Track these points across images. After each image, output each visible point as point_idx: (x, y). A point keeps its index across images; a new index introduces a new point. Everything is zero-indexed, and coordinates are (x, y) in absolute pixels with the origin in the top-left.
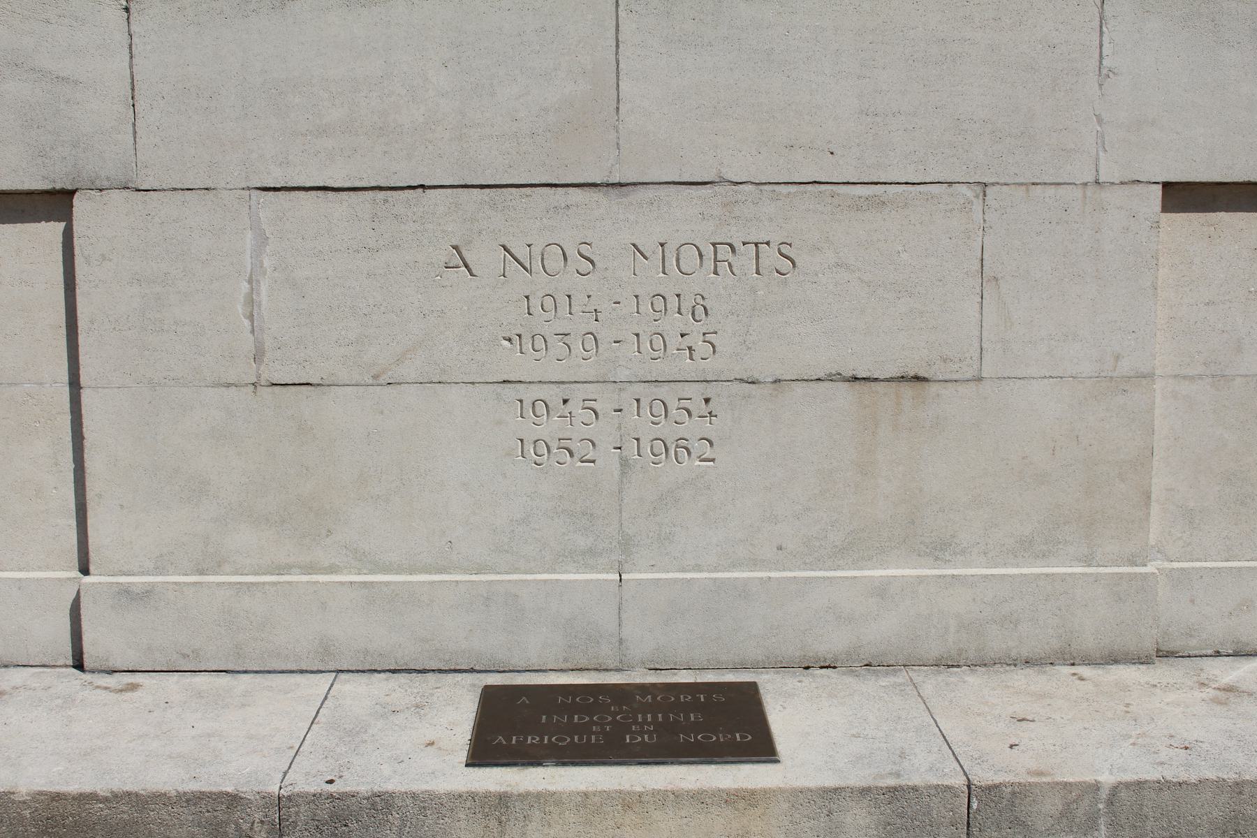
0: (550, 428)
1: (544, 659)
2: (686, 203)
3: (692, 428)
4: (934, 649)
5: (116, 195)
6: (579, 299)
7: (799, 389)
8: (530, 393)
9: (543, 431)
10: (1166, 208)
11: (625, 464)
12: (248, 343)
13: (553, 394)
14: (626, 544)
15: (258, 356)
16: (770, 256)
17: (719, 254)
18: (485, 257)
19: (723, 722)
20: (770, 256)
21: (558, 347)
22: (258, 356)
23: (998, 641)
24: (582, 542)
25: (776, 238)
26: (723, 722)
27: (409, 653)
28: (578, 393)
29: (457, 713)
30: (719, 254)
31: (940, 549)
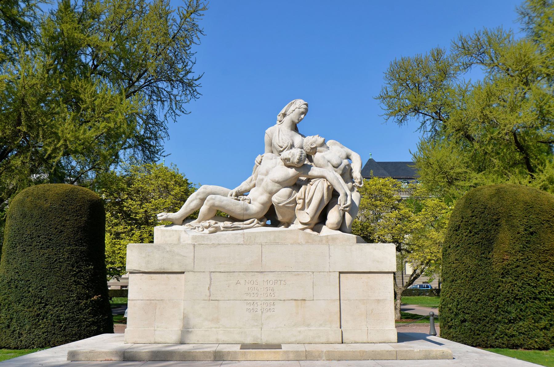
0: (251, 307)
1: (249, 340)
2: (271, 275)
4: (308, 341)
5: (191, 273)
6: (256, 288)
7: (287, 301)
8: (248, 302)
9: (250, 307)
10: (357, 242)
11: (262, 312)
12: (208, 294)
13: (252, 302)
14: (262, 324)
15: (210, 296)
17: (276, 282)
18: (242, 282)
19: (279, 347)
20: (283, 282)
21: (252, 295)
22: (210, 296)
23: (317, 340)
24: (256, 324)
25: (284, 279)
26: (279, 347)
27: (230, 341)
28: (255, 302)
29: (239, 346)
30: (276, 282)
31: (308, 325)
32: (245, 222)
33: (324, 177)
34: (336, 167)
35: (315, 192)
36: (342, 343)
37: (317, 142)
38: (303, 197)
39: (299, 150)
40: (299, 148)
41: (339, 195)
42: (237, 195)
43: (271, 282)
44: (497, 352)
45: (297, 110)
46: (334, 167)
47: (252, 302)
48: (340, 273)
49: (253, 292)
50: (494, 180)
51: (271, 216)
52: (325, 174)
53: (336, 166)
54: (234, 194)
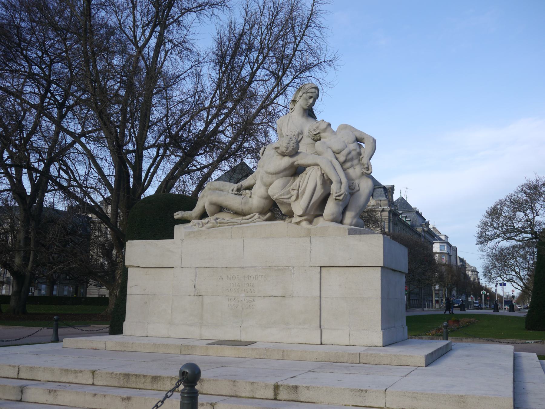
10: (349, 234)
11: (242, 309)
33: (317, 165)
34: (336, 153)
35: (310, 181)
36: (321, 344)
37: (320, 128)
38: (297, 187)
39: (355, 143)
40: (354, 142)
41: (331, 182)
42: (239, 190)
43: (252, 278)
44: (402, 345)
45: (305, 95)
46: (334, 152)
47: (233, 298)
48: (321, 267)
49: (234, 288)
50: (317, 138)
51: (274, 210)
52: (318, 162)
53: (337, 152)
54: (235, 189)
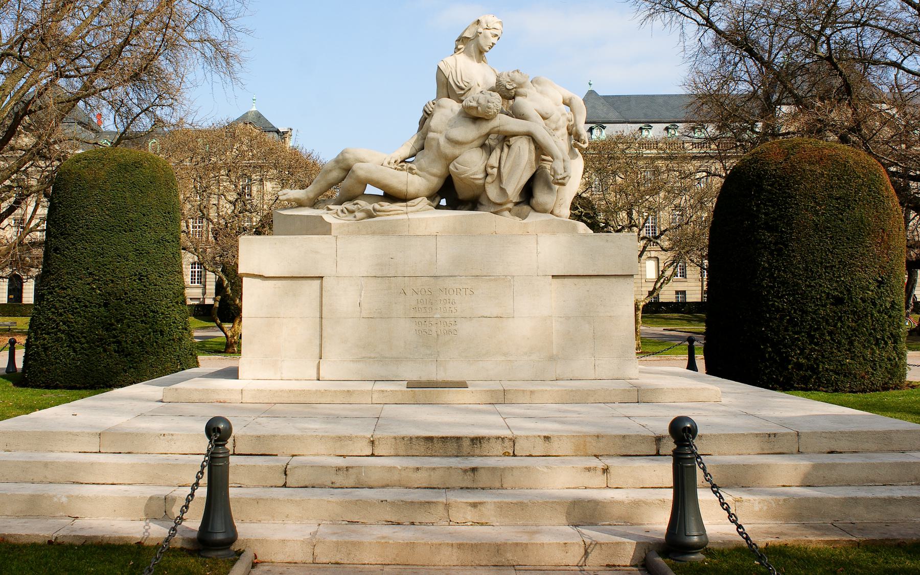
3: (453, 328)
16: (468, 291)
32: (409, 203)
38: (497, 165)
